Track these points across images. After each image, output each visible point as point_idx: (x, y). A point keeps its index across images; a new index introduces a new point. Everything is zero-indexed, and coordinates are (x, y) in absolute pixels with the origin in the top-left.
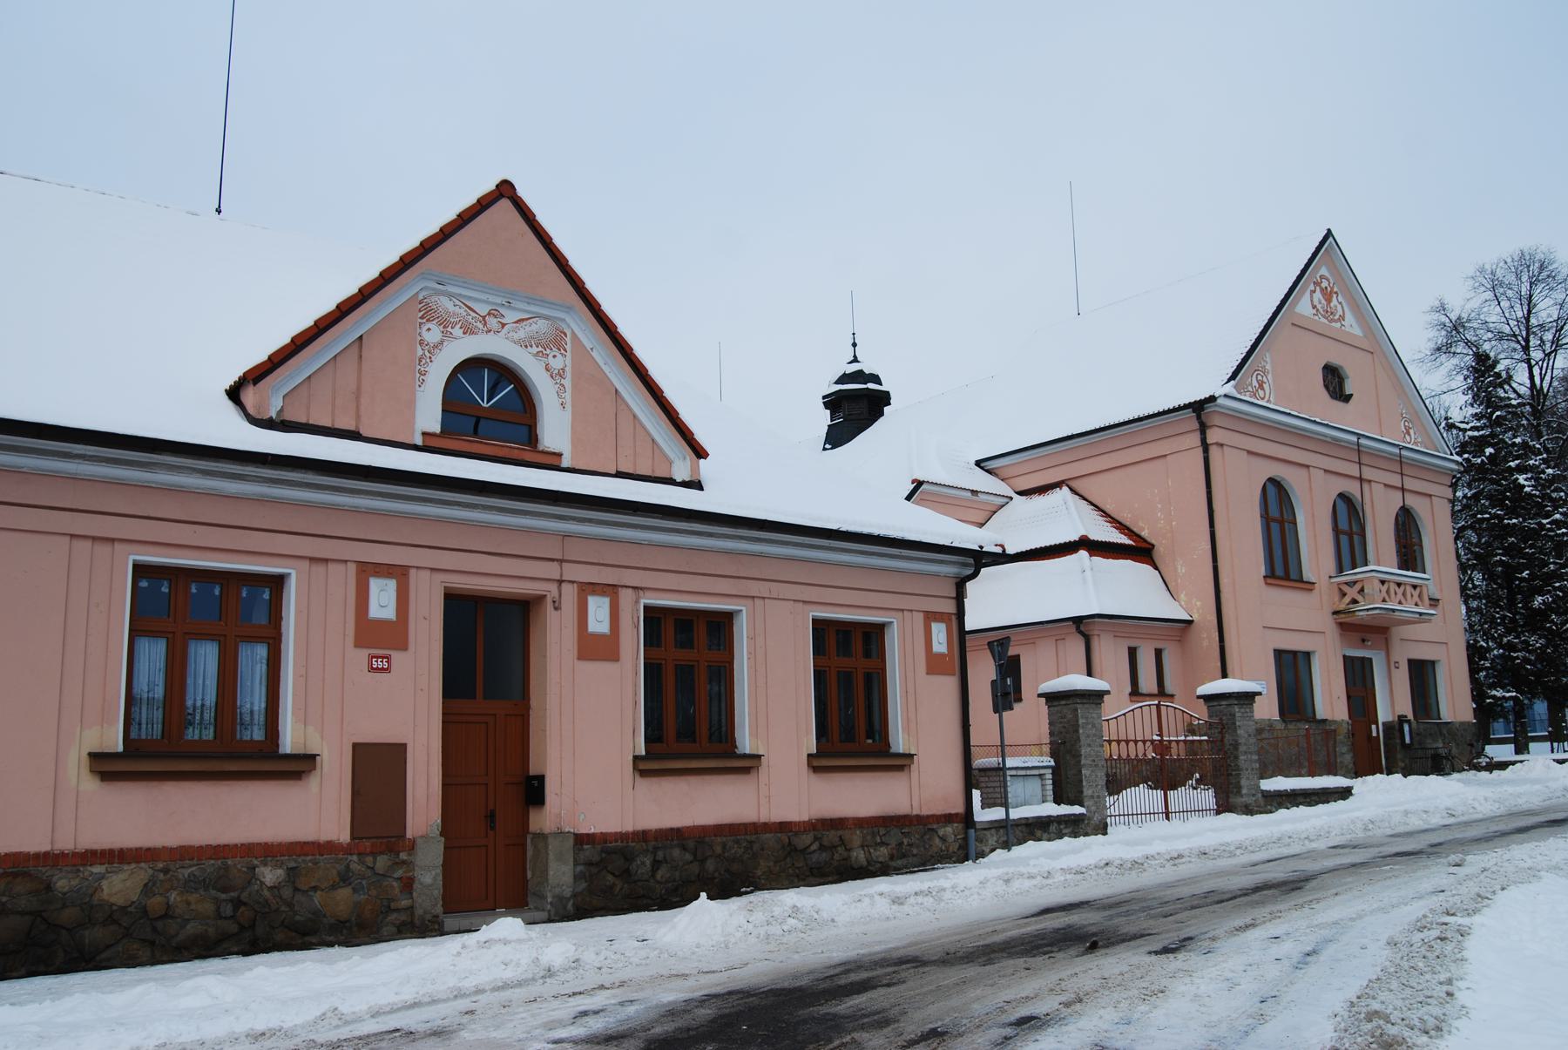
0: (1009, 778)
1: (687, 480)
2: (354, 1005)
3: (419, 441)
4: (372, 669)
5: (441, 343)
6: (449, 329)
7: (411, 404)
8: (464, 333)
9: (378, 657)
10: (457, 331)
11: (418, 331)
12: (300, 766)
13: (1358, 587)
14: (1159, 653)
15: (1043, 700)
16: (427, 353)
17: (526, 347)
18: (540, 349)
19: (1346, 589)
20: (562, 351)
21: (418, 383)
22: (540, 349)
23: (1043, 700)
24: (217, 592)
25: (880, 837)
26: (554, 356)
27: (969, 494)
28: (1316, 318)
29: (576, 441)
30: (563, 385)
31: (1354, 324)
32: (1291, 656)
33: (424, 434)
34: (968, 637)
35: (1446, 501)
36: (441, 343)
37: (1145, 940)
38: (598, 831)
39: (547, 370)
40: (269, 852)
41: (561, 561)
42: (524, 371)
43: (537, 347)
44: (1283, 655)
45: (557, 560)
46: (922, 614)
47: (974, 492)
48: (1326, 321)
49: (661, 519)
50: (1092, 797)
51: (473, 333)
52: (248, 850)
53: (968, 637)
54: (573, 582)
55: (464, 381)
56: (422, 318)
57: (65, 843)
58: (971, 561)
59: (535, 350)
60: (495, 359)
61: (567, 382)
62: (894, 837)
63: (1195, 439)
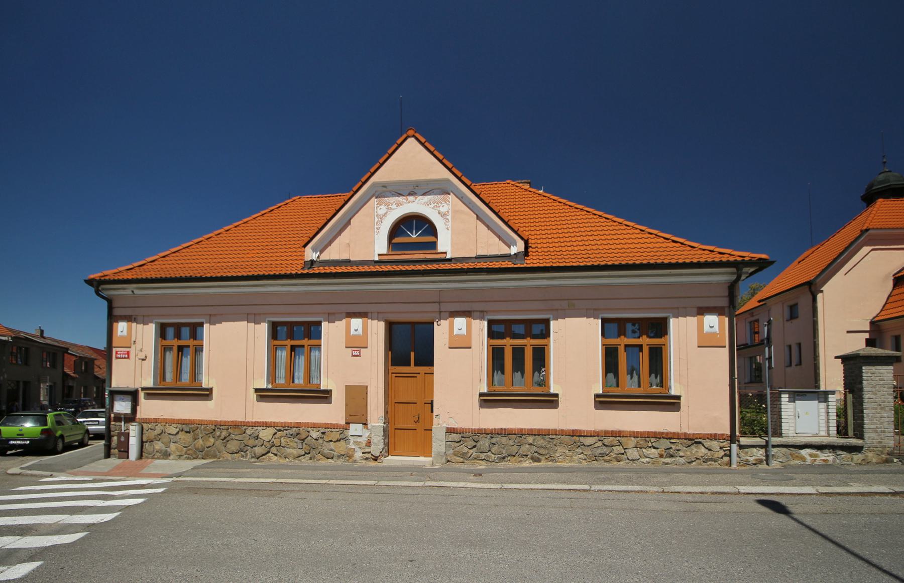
1: (516, 252)
2: (824, 441)
6: (390, 206)
7: (373, 243)
8: (397, 206)
9: (355, 351)
10: (394, 206)
11: (376, 210)
12: (324, 396)
15: (840, 360)
16: (379, 219)
17: (428, 205)
18: (435, 204)
20: (448, 203)
21: (376, 233)
22: (435, 204)
23: (840, 360)
24: (303, 329)
25: (652, 443)
26: (443, 206)
29: (453, 245)
30: (448, 219)
32: (606, 325)
33: (379, 255)
38: (459, 427)
39: (439, 214)
40: (315, 426)
42: (403, 215)
43: (434, 204)
44: (416, 326)
45: (437, 302)
46: (448, 313)
49: (486, 275)
52: (307, 425)
56: (377, 205)
57: (249, 419)
59: (433, 205)
60: (404, 216)
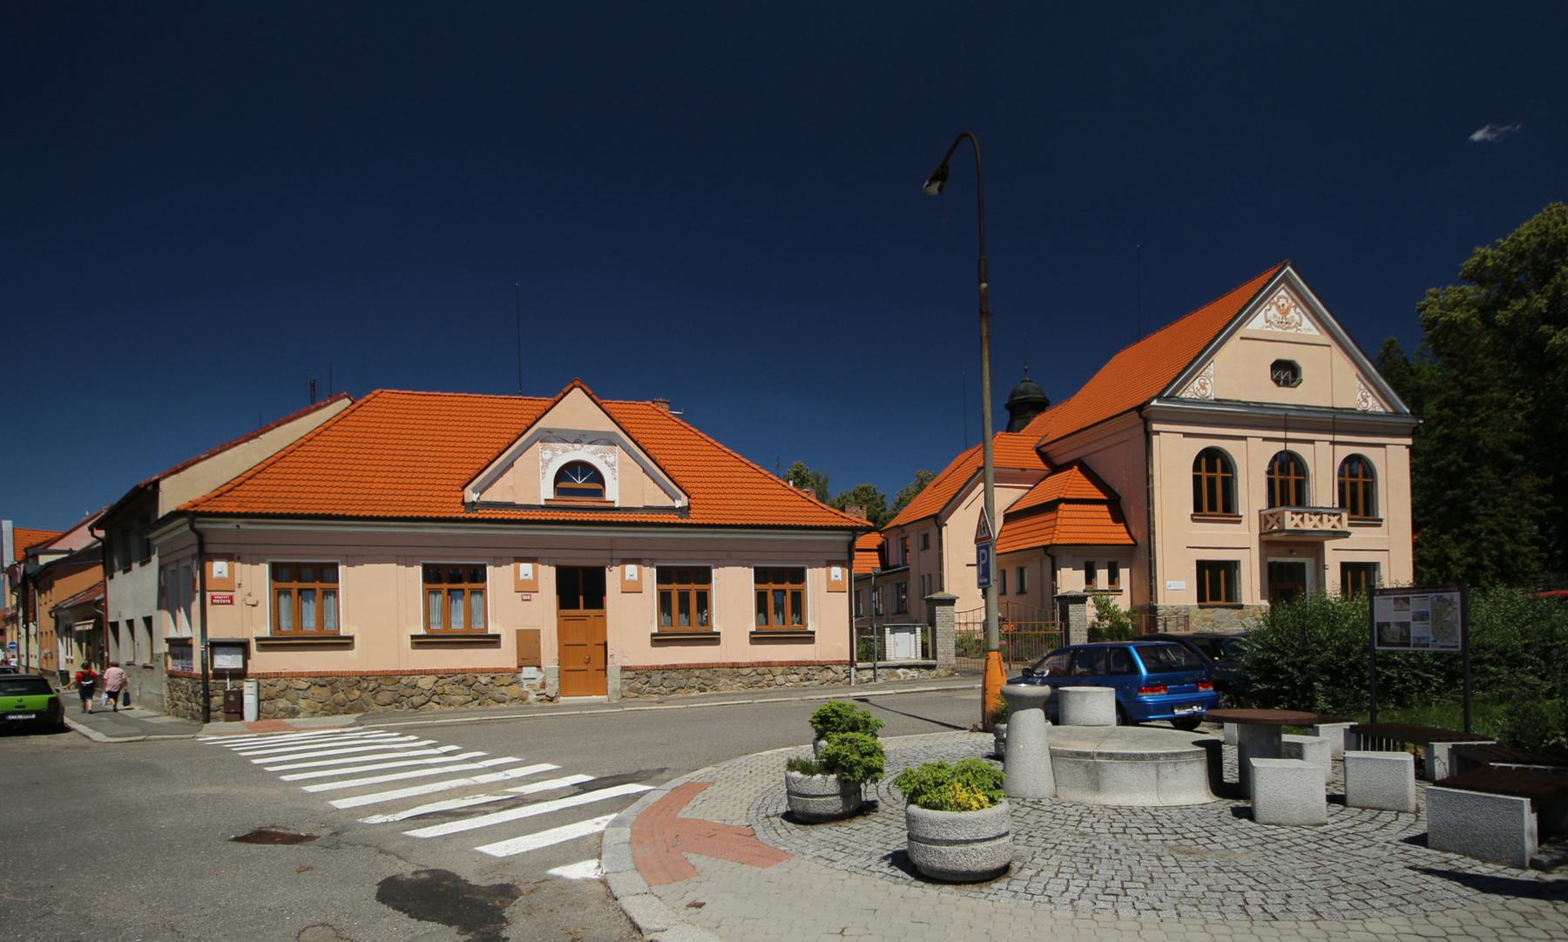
0: (1460, 644)
3: (543, 503)
4: (523, 600)
5: (552, 458)
12: (493, 641)
13: (1276, 517)
14: (1021, 571)
19: (1269, 518)
27: (1019, 471)
28: (1269, 329)
29: (621, 494)
31: (1312, 327)
33: (546, 500)
34: (975, 563)
35: (1404, 447)
36: (552, 458)
37: (223, 659)
41: (611, 550)
47: (1024, 470)
48: (1280, 330)
50: (944, 653)
51: (567, 451)
52: (474, 671)
53: (975, 563)
54: (618, 559)
55: (986, 365)
58: (851, 533)
61: (616, 468)
62: (804, 670)
63: (1141, 429)
